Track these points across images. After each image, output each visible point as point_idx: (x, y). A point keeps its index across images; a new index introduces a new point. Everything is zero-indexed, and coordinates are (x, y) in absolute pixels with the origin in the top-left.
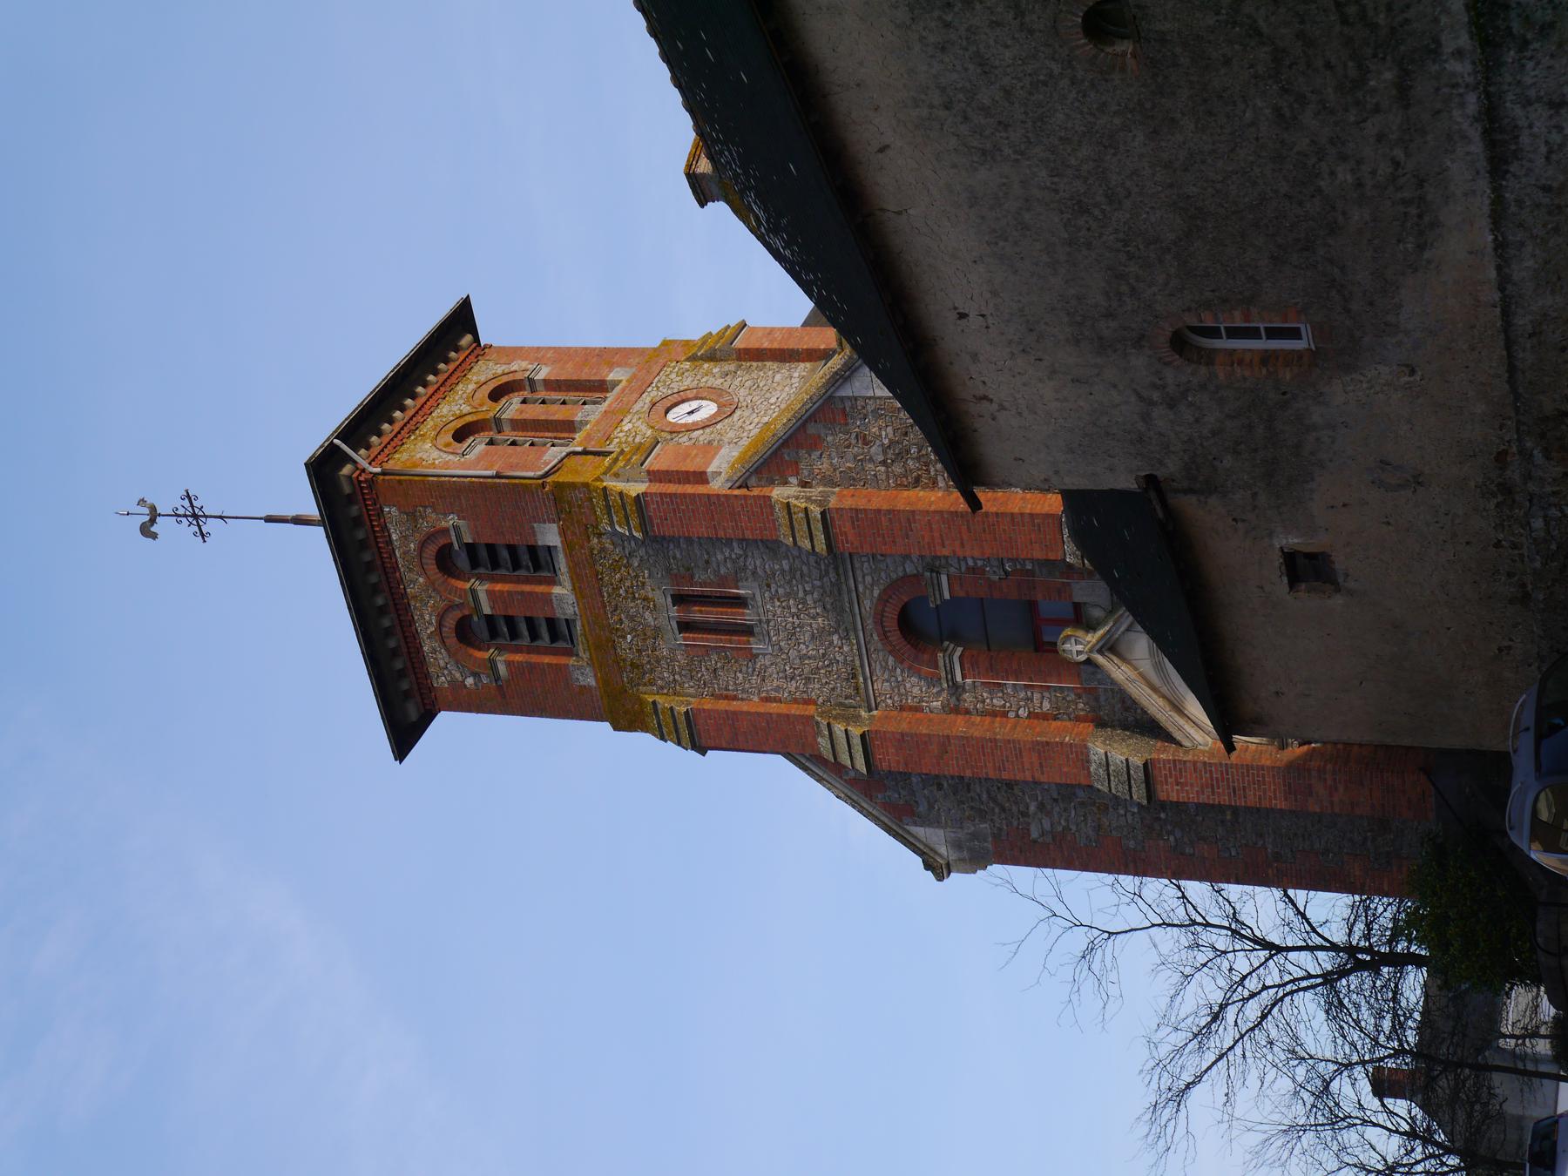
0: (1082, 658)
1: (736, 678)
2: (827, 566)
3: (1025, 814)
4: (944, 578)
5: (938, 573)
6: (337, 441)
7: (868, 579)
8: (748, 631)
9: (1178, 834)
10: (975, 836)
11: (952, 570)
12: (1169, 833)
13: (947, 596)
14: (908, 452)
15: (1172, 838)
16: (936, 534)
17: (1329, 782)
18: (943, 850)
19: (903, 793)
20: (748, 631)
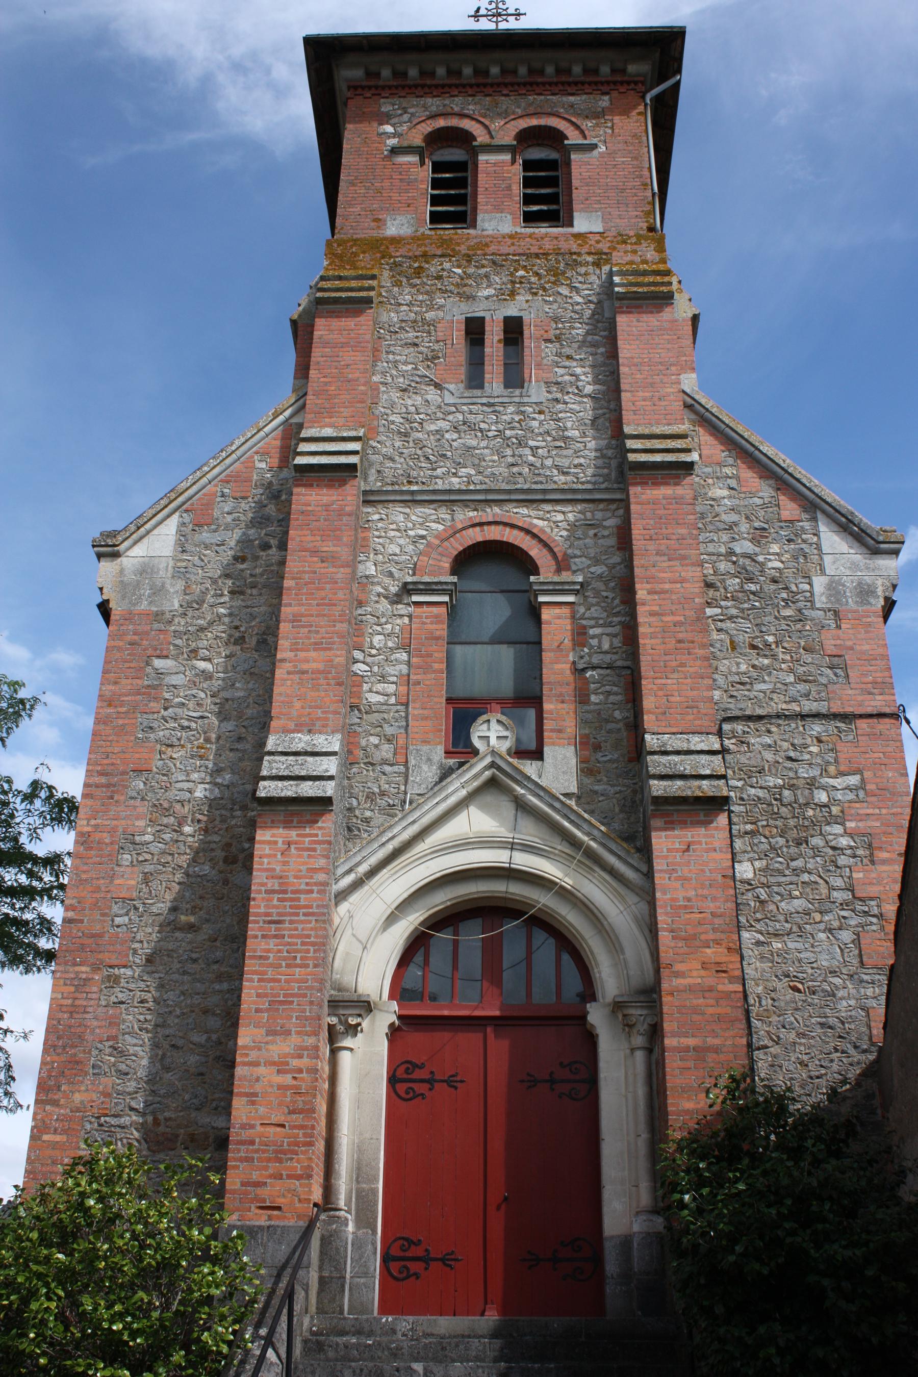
0: (477, 743)
1: (406, 363)
2: (575, 475)
3: (194, 653)
4: (571, 599)
5: (576, 592)
6: (529, 191)
7: (560, 517)
8: (475, 379)
9: (156, 848)
10: (158, 591)
11: (582, 610)
12: (157, 834)
13: (541, 599)
14: (750, 580)
15: (149, 838)
16: (667, 586)
17: (295, 1063)
18: (139, 551)
19: (229, 518)
20: (475, 379)
